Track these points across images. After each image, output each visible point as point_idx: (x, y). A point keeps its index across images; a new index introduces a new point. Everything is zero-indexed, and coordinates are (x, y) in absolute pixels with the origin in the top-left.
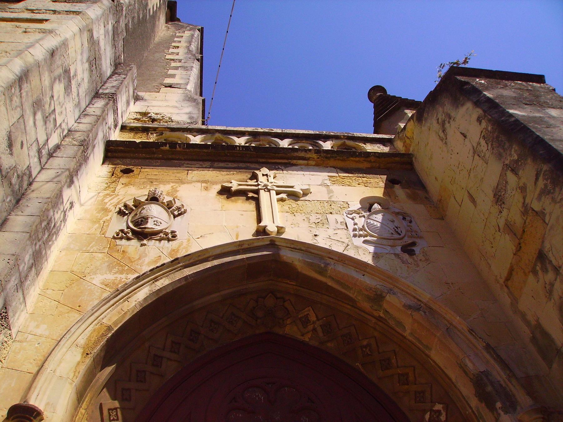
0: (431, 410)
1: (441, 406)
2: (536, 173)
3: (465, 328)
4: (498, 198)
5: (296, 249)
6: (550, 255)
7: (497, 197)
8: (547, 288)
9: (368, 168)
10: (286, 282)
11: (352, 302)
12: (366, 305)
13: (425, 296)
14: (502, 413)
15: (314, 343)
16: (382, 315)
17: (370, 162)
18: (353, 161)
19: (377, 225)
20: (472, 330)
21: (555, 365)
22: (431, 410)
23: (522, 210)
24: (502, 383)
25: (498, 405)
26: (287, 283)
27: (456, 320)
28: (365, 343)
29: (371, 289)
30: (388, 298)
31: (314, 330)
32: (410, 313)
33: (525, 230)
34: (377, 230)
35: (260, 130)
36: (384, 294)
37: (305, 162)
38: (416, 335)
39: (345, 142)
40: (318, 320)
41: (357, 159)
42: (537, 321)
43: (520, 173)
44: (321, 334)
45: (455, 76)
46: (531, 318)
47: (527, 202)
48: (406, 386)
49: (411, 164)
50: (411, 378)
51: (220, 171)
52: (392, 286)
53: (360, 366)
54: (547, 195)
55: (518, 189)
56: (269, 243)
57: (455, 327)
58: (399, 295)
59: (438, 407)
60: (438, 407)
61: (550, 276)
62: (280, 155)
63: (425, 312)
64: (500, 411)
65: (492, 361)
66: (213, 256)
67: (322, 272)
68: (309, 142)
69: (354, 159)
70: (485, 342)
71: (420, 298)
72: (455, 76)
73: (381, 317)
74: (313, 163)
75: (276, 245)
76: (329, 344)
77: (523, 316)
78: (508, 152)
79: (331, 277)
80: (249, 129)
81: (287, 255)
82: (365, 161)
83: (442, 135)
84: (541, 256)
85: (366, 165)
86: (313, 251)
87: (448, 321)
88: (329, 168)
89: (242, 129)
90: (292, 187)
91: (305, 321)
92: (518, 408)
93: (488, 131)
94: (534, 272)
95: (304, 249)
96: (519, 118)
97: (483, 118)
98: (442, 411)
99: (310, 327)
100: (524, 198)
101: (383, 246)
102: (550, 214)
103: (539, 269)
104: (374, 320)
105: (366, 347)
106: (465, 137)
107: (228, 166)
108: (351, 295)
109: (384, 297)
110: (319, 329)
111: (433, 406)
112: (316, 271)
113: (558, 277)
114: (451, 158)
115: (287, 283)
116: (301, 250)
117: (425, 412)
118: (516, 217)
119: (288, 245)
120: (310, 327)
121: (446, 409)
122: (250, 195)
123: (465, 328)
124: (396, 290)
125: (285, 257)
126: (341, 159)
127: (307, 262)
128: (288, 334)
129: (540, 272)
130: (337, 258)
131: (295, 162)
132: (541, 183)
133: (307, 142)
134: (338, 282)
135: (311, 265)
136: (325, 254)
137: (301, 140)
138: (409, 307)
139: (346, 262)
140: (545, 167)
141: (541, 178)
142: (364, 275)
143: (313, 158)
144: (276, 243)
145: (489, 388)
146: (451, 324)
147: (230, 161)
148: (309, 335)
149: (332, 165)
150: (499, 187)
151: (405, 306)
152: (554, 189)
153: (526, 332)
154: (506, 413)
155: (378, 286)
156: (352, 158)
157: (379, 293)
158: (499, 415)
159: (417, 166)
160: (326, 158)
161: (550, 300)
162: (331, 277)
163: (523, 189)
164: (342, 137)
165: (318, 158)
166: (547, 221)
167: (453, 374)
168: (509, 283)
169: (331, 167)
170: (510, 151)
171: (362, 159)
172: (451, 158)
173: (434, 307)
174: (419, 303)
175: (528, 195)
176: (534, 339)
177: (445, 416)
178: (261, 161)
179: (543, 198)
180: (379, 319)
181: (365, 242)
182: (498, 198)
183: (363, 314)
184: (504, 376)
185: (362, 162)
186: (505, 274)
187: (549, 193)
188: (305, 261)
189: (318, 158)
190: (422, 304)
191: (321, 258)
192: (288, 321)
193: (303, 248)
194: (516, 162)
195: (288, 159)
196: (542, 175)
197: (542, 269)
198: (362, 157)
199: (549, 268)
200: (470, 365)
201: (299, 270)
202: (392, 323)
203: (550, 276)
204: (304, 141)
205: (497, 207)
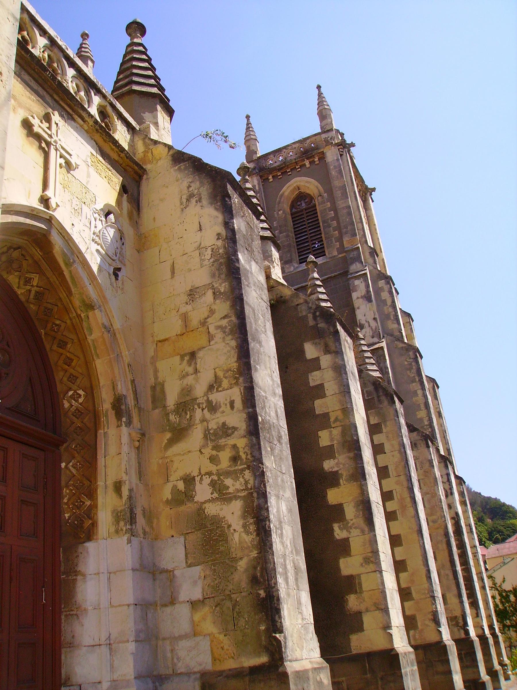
0: (75, 391)
1: (84, 393)
2: (226, 314)
3: (127, 361)
4: (191, 295)
5: (61, 234)
6: (198, 361)
7: (192, 293)
8: (183, 373)
9: (115, 160)
10: (36, 249)
11: (70, 293)
12: (77, 303)
13: (117, 325)
14: (124, 425)
15: (23, 298)
16: (82, 315)
17: (119, 155)
18: (110, 146)
19: (109, 240)
20: (130, 365)
21: (157, 411)
22: (75, 391)
23: (202, 321)
24: (130, 406)
25: (124, 419)
26: (36, 250)
27: (125, 353)
28: (58, 322)
29: (90, 298)
30: (96, 311)
31: (30, 291)
32: (103, 330)
33: (194, 331)
34: (107, 244)
35: (60, 43)
36: (95, 308)
37: (82, 123)
38: (95, 344)
39: (107, 106)
40: (37, 286)
41: (114, 147)
42: (164, 382)
43: (217, 301)
44: (32, 296)
45: (228, 184)
46: (160, 375)
47: (208, 320)
48: (67, 367)
49: (141, 177)
50: (73, 364)
51: (25, 88)
52: (102, 304)
53: (43, 334)
54: (223, 332)
55: (209, 307)
56: (48, 218)
57: (122, 357)
58: (103, 313)
59: (81, 392)
60: (81, 392)
61: (190, 370)
62: (70, 102)
63: (111, 336)
64: (123, 423)
65: (131, 391)
66: (15, 211)
67: (68, 264)
68: (84, 85)
69: (112, 145)
70: (133, 377)
71: (113, 324)
72: (228, 184)
73: (81, 317)
74: (86, 128)
75: (51, 222)
76: (32, 306)
77: (156, 371)
78: (220, 281)
79: (70, 272)
80: (52, 32)
81: (55, 238)
82: (117, 152)
83: (184, 201)
84: (193, 355)
85: (114, 156)
86: (70, 244)
87: (120, 350)
88: (93, 141)
89: (47, 26)
90: (70, 155)
91: (28, 281)
92: (132, 426)
93: (218, 251)
94: (182, 357)
95: (66, 238)
96: (241, 268)
97: (222, 239)
98: (82, 396)
99: (28, 287)
100: (208, 317)
101: (104, 261)
102: (216, 343)
103: (186, 360)
104: (75, 314)
105: (56, 325)
106: (201, 230)
107: (30, 83)
108: (73, 290)
109: (94, 310)
110: (33, 292)
111: (78, 390)
112: (64, 261)
113: (194, 375)
114: (178, 225)
115: (36, 250)
116: (64, 237)
117: (70, 389)
118: (195, 318)
119: (58, 228)
120: (28, 287)
121: (86, 397)
122: (44, 145)
123: (127, 361)
124: (103, 308)
125: (52, 238)
126: (105, 138)
127: (64, 251)
128: (8, 280)
129: (185, 362)
130: (81, 260)
131: (76, 117)
132: (224, 322)
133: (83, 83)
134: (72, 277)
135: (64, 254)
136: (76, 252)
137: (81, 78)
138: (105, 327)
139: (85, 267)
140: (233, 319)
141: (226, 320)
142: (90, 284)
143: (89, 123)
144: (52, 221)
145: (123, 407)
146: (121, 353)
147: (36, 81)
148: (23, 291)
149: (96, 139)
150: (198, 290)
151: (103, 324)
152: (229, 334)
153: (152, 381)
154: (126, 426)
155: (95, 300)
156: (111, 144)
157: (93, 304)
158: (121, 425)
159: (144, 183)
160: (97, 130)
161: (180, 380)
162: (70, 272)
163: (212, 312)
164: (108, 100)
165: (92, 126)
166: (212, 343)
167: (103, 381)
168: (159, 344)
169: (94, 141)
170: (222, 282)
171: (117, 150)
172: (178, 225)
173: (117, 336)
174: (111, 327)
175: (212, 318)
176: (153, 388)
177: (82, 400)
178: (55, 97)
179: (219, 330)
180: (79, 316)
181: (97, 251)
182: (191, 295)
183: (71, 306)
184: (133, 404)
185: (115, 152)
186: (162, 338)
187: (224, 332)
188: (63, 250)
189: (92, 126)
190: (112, 329)
191: (73, 253)
192: (17, 273)
193: (66, 237)
194: (221, 293)
195: (73, 110)
196: (229, 319)
197: (188, 361)
198: (118, 149)
199: (193, 365)
200: (119, 387)
201: (54, 252)
202: (85, 324)
203: (190, 370)
204: (82, 81)
205: (186, 297)
